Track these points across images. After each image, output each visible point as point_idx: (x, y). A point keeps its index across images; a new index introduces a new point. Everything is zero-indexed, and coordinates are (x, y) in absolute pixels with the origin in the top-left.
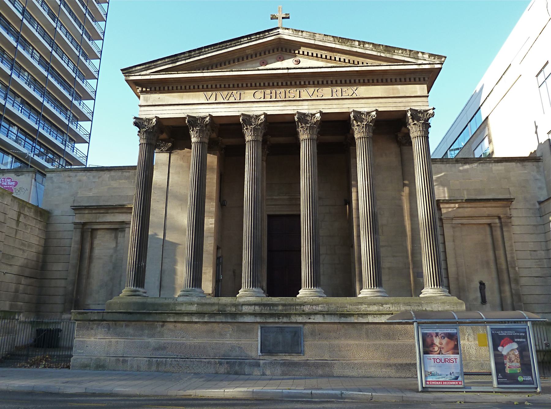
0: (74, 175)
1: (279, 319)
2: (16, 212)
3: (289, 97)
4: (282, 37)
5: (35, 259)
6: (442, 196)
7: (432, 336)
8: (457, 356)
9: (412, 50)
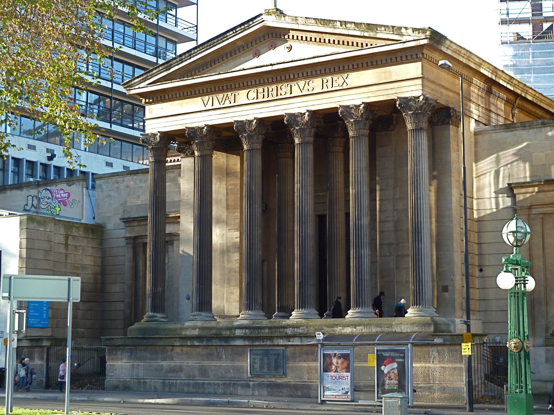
0: (122, 180)
1: (263, 342)
2: (62, 236)
3: (281, 94)
4: (265, 24)
5: (92, 281)
6: (522, 175)
7: (331, 357)
8: (349, 374)
9: (394, 25)
